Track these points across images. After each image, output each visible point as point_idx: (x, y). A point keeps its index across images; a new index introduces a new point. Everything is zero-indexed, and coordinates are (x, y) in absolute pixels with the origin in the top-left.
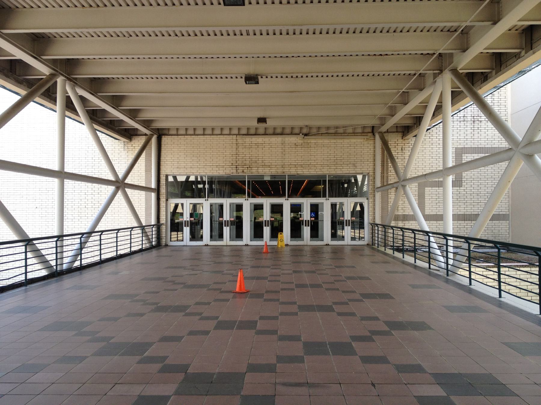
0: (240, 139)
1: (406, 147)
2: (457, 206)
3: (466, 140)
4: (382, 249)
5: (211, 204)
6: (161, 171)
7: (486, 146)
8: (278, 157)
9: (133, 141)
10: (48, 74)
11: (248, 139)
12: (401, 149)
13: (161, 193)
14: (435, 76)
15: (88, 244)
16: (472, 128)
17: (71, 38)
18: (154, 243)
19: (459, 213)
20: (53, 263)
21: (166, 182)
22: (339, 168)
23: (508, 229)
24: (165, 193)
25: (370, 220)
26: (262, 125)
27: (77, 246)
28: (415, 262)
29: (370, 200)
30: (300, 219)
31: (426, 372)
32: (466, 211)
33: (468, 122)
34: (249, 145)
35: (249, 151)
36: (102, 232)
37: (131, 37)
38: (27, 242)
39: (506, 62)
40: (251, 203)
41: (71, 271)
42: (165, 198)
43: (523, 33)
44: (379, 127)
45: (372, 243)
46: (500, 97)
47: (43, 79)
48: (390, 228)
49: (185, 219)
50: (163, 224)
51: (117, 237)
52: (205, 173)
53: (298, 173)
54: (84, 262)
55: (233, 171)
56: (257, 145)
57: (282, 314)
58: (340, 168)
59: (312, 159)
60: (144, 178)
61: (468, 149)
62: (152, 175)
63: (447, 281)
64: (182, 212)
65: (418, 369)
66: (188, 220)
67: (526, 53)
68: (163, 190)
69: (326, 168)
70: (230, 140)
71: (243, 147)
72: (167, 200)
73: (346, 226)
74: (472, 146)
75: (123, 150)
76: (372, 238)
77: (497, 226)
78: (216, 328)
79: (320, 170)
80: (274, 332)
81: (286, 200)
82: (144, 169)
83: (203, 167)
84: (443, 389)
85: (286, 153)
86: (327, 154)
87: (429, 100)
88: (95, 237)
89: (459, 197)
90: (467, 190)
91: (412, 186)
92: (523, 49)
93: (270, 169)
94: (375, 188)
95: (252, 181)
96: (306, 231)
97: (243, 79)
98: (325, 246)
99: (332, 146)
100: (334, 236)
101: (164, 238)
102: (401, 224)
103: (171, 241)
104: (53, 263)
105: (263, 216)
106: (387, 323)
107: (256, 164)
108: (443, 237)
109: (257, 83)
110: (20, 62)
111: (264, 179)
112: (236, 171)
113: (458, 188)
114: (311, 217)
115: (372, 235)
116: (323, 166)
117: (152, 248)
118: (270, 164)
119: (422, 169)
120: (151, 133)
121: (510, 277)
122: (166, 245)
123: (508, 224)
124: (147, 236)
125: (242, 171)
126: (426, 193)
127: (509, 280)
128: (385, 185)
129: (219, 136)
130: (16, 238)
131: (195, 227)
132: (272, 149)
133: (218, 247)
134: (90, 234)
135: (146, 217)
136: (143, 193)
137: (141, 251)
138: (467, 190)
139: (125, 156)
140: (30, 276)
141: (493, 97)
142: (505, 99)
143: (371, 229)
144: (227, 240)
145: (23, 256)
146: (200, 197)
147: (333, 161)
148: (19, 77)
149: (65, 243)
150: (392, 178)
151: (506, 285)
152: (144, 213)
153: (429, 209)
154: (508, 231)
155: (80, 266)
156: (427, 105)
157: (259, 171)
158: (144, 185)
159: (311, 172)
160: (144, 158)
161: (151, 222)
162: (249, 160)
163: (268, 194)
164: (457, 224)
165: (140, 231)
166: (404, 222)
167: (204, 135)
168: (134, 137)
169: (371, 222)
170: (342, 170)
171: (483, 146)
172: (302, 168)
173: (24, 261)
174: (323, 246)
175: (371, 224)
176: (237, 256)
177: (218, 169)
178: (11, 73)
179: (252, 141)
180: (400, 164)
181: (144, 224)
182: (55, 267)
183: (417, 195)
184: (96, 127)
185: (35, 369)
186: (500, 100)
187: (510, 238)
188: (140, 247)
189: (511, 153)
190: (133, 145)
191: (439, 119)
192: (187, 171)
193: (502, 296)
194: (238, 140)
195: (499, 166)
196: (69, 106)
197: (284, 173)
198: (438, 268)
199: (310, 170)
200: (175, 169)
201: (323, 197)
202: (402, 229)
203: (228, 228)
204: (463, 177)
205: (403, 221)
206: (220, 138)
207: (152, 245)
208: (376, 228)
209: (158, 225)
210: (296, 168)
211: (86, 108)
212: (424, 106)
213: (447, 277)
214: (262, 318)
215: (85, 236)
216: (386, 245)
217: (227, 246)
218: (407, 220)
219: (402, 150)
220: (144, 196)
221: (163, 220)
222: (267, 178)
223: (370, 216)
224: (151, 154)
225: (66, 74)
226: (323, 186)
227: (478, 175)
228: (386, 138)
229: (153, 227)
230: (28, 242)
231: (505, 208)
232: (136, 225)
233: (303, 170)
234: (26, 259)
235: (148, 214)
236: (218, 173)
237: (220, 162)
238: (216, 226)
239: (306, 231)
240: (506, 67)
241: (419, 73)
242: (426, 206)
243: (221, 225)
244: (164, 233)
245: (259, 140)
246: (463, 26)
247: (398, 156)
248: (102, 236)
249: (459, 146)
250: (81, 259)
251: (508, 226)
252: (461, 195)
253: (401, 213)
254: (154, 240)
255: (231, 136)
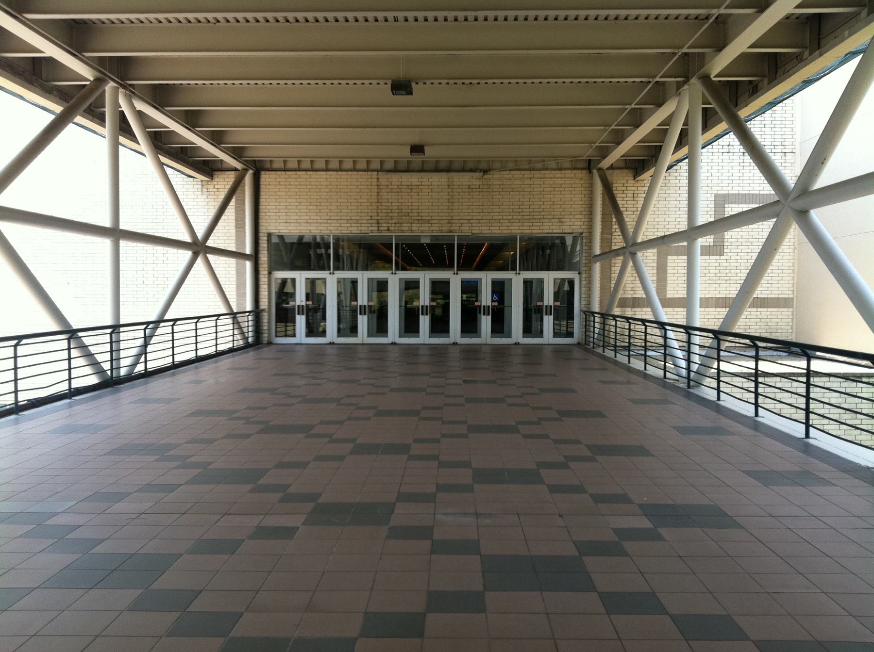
0: (384, 178)
1: (640, 192)
2: (715, 285)
3: (731, 182)
4: (600, 350)
5: (339, 280)
6: (261, 228)
7: (762, 192)
8: (441, 207)
9: (217, 180)
10: (92, 79)
11: (395, 178)
12: (632, 195)
13: (260, 262)
14: (679, 86)
15: (154, 340)
16: (741, 164)
17: (128, 24)
18: (250, 340)
19: (718, 296)
20: (107, 366)
21: (268, 244)
22: (536, 224)
23: (790, 320)
24: (266, 262)
25: (583, 306)
26: (417, 158)
27: (141, 342)
28: (645, 369)
29: (584, 275)
30: (476, 304)
31: (633, 503)
32: (728, 292)
33: (735, 154)
34: (397, 187)
35: (396, 197)
36: (175, 320)
37: (218, 24)
38: (70, 334)
39: (784, 65)
40: (400, 279)
41: (131, 378)
42: (267, 269)
43: (807, 23)
44: (599, 161)
45: (585, 342)
46: (784, 115)
47: (86, 87)
48: (611, 318)
49: (298, 302)
50: (264, 310)
51: (15, 357)
52: (329, 232)
53: (473, 232)
54: (151, 365)
55: (373, 228)
56: (410, 187)
57: (444, 436)
58: (539, 224)
59: (494, 210)
60: (234, 238)
61: (734, 196)
62: (245, 233)
63: (689, 396)
64: (293, 291)
65: (624, 499)
66: (304, 303)
67: (810, 54)
68: (264, 257)
69: (517, 224)
70: (368, 179)
71: (388, 190)
72: (270, 273)
73: (546, 314)
74: (741, 192)
75: (200, 193)
76: (585, 334)
77: (774, 317)
78: (353, 452)
79: (508, 228)
80: (435, 458)
81: (454, 274)
82: (234, 224)
83: (326, 221)
84: (650, 520)
85: (455, 200)
86: (519, 203)
87: (670, 122)
88: (164, 329)
89: (718, 271)
90: (731, 261)
91: (648, 254)
92: (806, 48)
93: (429, 225)
94: (593, 256)
95: (402, 244)
96: (486, 322)
97: (389, 86)
98: (514, 346)
99: (526, 190)
100: (528, 330)
101: (266, 332)
102: (629, 313)
103: (276, 336)
104: (107, 366)
105: (418, 298)
106: (589, 447)
107: (408, 218)
108: (684, 331)
109: (411, 93)
110: (50, 60)
111: (420, 241)
112: (376, 228)
113: (718, 257)
114: (493, 301)
115: (586, 328)
116: (511, 221)
117: (247, 346)
118: (430, 218)
119: (663, 227)
120: (245, 167)
121: (782, 391)
122: (270, 343)
123: (791, 313)
124: (240, 328)
125: (386, 228)
126: (669, 264)
127: (793, 399)
128: (608, 253)
129: (350, 173)
130: (56, 328)
131: (313, 316)
132: (433, 194)
133: (349, 346)
134: (157, 323)
135: (237, 300)
136: (232, 261)
137: (231, 351)
138: (731, 261)
139: (203, 204)
140: (76, 384)
141: (773, 115)
142: (792, 119)
143: (584, 320)
144: (363, 335)
145: (65, 355)
146: (322, 268)
147: (528, 214)
148: (46, 83)
149: (123, 336)
150: (618, 242)
151: (776, 402)
152: (235, 293)
153: (672, 289)
154: (790, 324)
155: (143, 372)
156: (668, 129)
157: (413, 228)
158: (234, 249)
159: (493, 232)
160: (234, 207)
161: (245, 307)
162: (397, 211)
163: (426, 264)
164: (715, 313)
165: (230, 321)
166: (634, 309)
167: (327, 170)
168: (217, 173)
169: (585, 309)
170: (542, 228)
171: (757, 192)
172: (479, 225)
173: (171, 342)
174: (509, 346)
175: (584, 312)
176: (379, 359)
177: (349, 225)
178: (35, 77)
179: (401, 182)
180: (630, 220)
181: (235, 311)
182: (109, 373)
183: (655, 268)
184: (163, 159)
185: (120, 497)
186: (783, 119)
187: (794, 334)
188: (230, 345)
189: (777, 208)
190: (216, 187)
191: (685, 151)
192: (300, 228)
193: (760, 414)
194: (380, 180)
195: (749, 230)
196: (123, 128)
197: (451, 232)
198: (677, 378)
199: (491, 228)
200: (281, 224)
201: (512, 270)
202: (628, 319)
203: (365, 317)
204: (725, 240)
205: (633, 307)
206: (353, 176)
207: (248, 343)
208: (592, 318)
209: (257, 312)
210: (470, 225)
211: (147, 130)
212: (662, 133)
213: (688, 390)
214: (416, 441)
215: (151, 326)
216: (606, 344)
217: (363, 344)
218: (639, 307)
219: (634, 197)
220: (235, 266)
221: (264, 303)
222: (425, 241)
223: (583, 299)
224: (244, 200)
225: (118, 78)
226: (512, 253)
227: (748, 237)
228: (609, 178)
229: (249, 315)
230: (72, 334)
231: (787, 289)
232: (224, 310)
233: (481, 228)
234: (69, 359)
235: (241, 295)
236: (350, 232)
237: (352, 214)
238: (347, 314)
239: (486, 322)
240: (784, 74)
241: (655, 81)
242: (668, 285)
243: (354, 312)
244: (266, 324)
245: (413, 179)
246: (714, 14)
247: (626, 206)
248: (174, 327)
249: (720, 192)
250: (146, 362)
251: (791, 317)
252: (722, 268)
253: (630, 296)
254: (250, 334)
255: (369, 173)
